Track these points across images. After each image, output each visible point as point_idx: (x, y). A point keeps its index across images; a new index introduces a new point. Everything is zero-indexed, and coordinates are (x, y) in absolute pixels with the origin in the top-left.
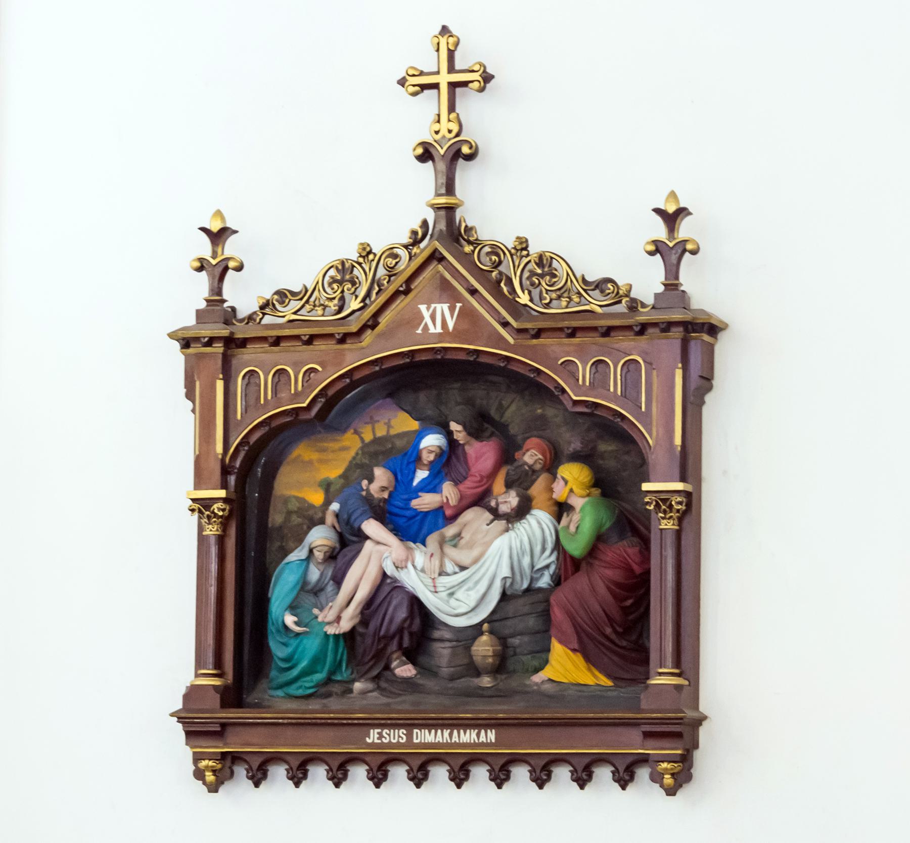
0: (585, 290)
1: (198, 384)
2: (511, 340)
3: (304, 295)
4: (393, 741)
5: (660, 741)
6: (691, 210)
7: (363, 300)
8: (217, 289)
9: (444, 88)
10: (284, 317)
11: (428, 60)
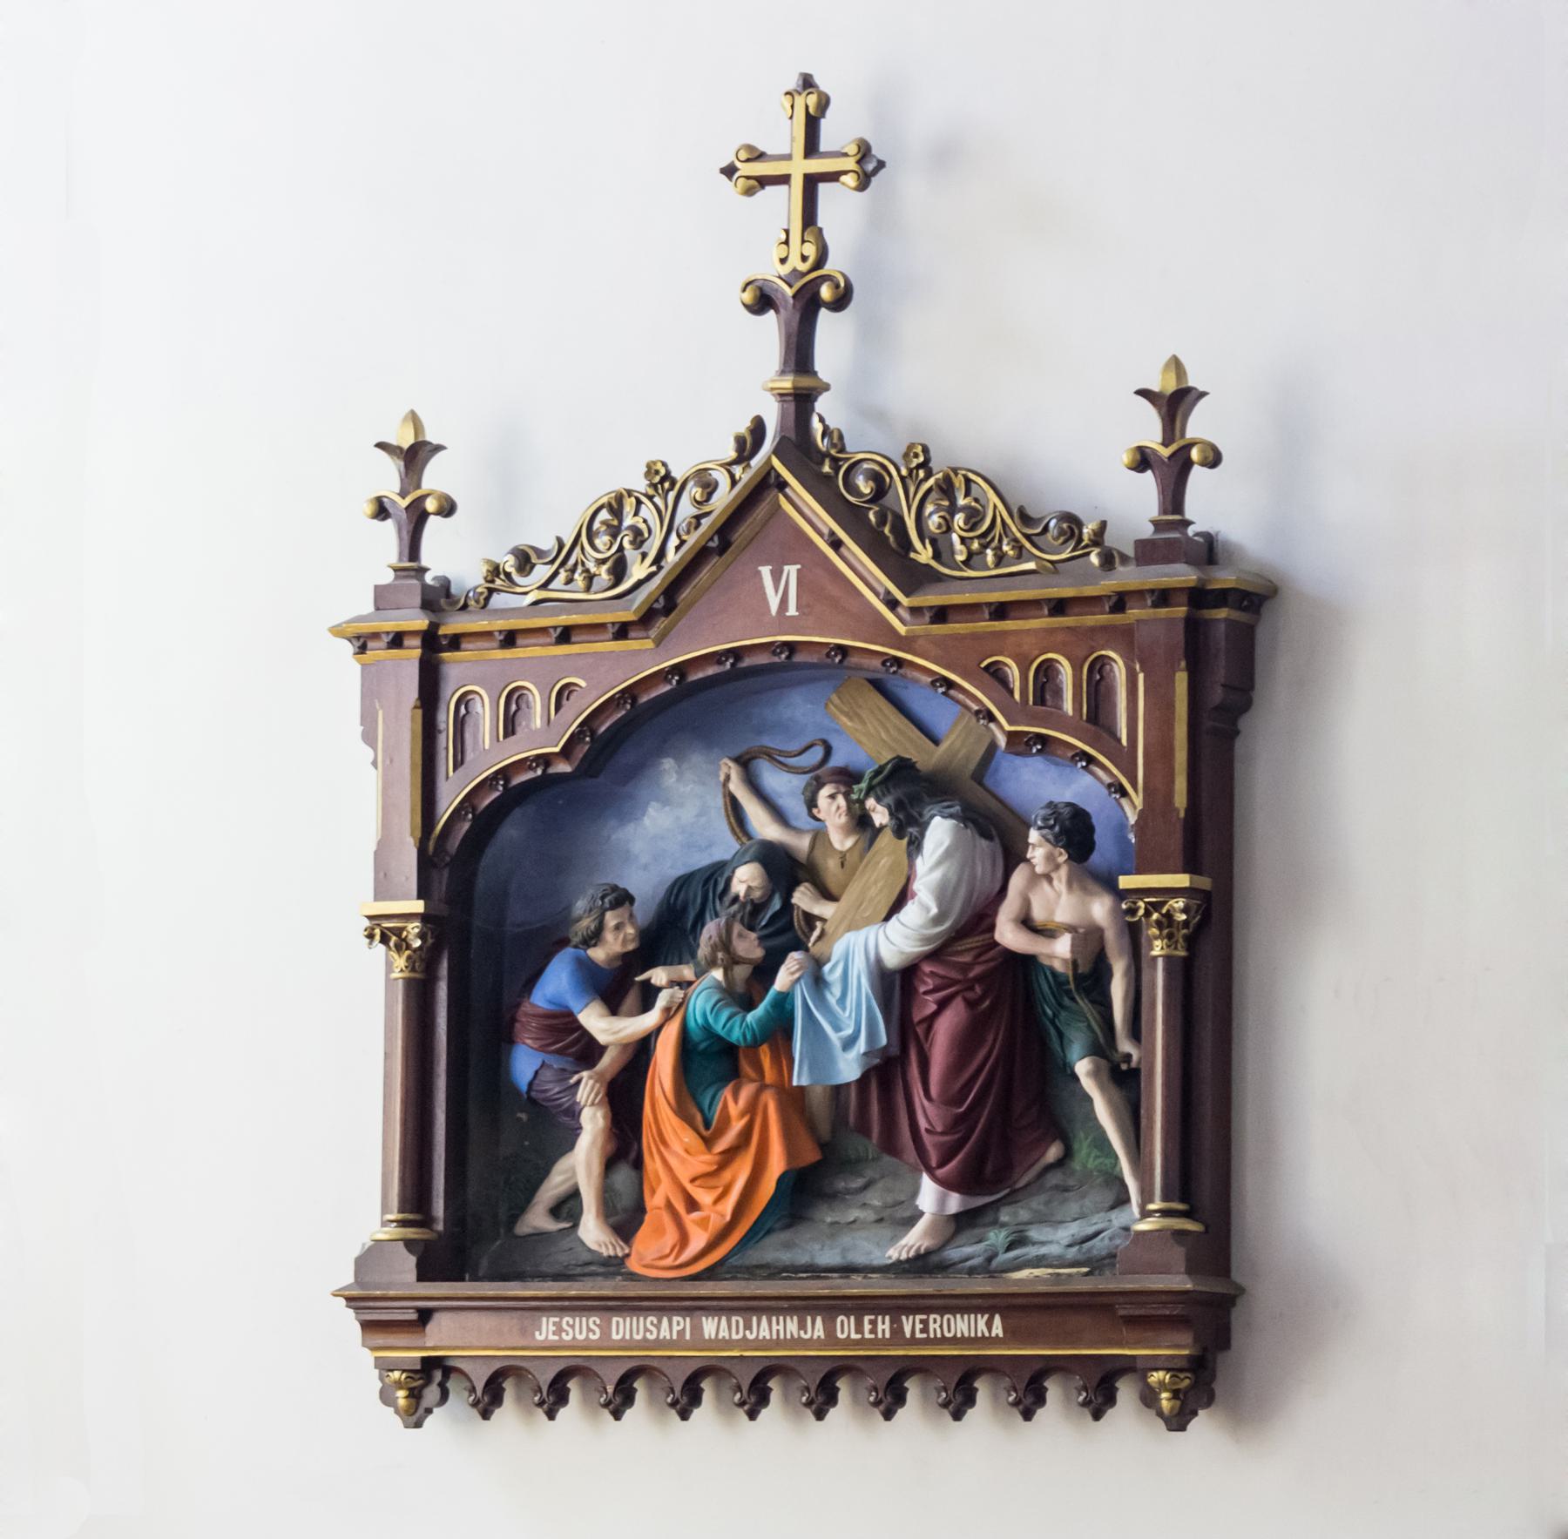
0: (1028, 537)
1: (380, 713)
2: (902, 630)
3: (563, 556)
4: (947, 1335)
5: (1189, 1331)
9: (797, 183)
10: (526, 593)
11: (780, 135)
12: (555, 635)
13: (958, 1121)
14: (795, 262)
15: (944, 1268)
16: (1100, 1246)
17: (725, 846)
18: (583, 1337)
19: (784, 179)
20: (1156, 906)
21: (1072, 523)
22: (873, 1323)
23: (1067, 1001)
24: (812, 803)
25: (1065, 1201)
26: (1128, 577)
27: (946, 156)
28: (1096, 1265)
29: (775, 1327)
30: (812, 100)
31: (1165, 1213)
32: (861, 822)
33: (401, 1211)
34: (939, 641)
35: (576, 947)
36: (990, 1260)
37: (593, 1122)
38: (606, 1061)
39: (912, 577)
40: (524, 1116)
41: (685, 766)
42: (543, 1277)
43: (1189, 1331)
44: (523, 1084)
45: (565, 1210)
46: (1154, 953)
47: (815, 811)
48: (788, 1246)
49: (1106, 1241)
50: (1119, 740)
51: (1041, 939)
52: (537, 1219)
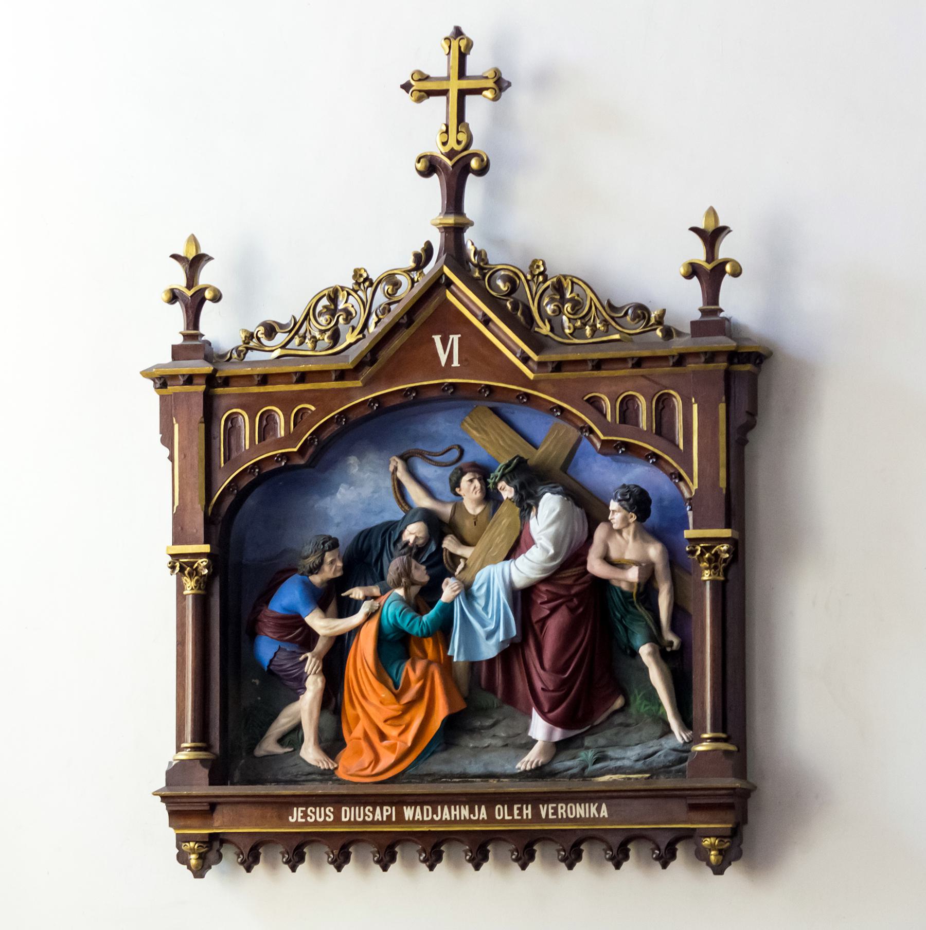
0: (613, 318)
2: (531, 376)
3: (295, 329)
4: (358, 819)
5: (722, 812)
6: (210, 255)
7: (361, 332)
8: (193, 318)
9: (453, 95)
10: (272, 351)
11: (439, 65)
12: (295, 379)
13: (564, 682)
14: (452, 144)
15: (553, 775)
16: (659, 760)
17: (395, 513)
18: (361, 819)
19: (444, 92)
20: (708, 549)
21: (641, 312)
22: (520, 809)
23: (631, 609)
24: (455, 484)
25: (627, 733)
26: (678, 345)
27: (545, 80)
28: (654, 772)
29: (453, 813)
30: (463, 43)
31: (713, 740)
32: (490, 497)
33: (193, 741)
34: (555, 383)
35: (302, 574)
36: (584, 769)
37: (314, 685)
38: (320, 646)
39: (538, 343)
40: (257, 682)
41: (364, 461)
42: (278, 782)
43: (722, 812)
44: (266, 663)
45: (287, 740)
46: (185, 593)
47: (457, 490)
48: (447, 762)
49: (662, 758)
50: (678, 446)
51: (618, 570)
52: (269, 746)
